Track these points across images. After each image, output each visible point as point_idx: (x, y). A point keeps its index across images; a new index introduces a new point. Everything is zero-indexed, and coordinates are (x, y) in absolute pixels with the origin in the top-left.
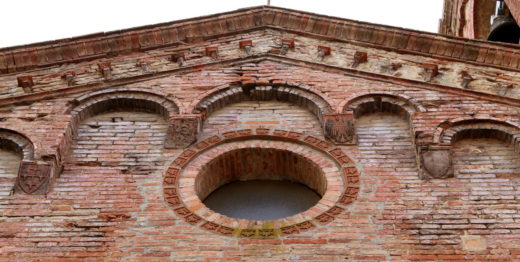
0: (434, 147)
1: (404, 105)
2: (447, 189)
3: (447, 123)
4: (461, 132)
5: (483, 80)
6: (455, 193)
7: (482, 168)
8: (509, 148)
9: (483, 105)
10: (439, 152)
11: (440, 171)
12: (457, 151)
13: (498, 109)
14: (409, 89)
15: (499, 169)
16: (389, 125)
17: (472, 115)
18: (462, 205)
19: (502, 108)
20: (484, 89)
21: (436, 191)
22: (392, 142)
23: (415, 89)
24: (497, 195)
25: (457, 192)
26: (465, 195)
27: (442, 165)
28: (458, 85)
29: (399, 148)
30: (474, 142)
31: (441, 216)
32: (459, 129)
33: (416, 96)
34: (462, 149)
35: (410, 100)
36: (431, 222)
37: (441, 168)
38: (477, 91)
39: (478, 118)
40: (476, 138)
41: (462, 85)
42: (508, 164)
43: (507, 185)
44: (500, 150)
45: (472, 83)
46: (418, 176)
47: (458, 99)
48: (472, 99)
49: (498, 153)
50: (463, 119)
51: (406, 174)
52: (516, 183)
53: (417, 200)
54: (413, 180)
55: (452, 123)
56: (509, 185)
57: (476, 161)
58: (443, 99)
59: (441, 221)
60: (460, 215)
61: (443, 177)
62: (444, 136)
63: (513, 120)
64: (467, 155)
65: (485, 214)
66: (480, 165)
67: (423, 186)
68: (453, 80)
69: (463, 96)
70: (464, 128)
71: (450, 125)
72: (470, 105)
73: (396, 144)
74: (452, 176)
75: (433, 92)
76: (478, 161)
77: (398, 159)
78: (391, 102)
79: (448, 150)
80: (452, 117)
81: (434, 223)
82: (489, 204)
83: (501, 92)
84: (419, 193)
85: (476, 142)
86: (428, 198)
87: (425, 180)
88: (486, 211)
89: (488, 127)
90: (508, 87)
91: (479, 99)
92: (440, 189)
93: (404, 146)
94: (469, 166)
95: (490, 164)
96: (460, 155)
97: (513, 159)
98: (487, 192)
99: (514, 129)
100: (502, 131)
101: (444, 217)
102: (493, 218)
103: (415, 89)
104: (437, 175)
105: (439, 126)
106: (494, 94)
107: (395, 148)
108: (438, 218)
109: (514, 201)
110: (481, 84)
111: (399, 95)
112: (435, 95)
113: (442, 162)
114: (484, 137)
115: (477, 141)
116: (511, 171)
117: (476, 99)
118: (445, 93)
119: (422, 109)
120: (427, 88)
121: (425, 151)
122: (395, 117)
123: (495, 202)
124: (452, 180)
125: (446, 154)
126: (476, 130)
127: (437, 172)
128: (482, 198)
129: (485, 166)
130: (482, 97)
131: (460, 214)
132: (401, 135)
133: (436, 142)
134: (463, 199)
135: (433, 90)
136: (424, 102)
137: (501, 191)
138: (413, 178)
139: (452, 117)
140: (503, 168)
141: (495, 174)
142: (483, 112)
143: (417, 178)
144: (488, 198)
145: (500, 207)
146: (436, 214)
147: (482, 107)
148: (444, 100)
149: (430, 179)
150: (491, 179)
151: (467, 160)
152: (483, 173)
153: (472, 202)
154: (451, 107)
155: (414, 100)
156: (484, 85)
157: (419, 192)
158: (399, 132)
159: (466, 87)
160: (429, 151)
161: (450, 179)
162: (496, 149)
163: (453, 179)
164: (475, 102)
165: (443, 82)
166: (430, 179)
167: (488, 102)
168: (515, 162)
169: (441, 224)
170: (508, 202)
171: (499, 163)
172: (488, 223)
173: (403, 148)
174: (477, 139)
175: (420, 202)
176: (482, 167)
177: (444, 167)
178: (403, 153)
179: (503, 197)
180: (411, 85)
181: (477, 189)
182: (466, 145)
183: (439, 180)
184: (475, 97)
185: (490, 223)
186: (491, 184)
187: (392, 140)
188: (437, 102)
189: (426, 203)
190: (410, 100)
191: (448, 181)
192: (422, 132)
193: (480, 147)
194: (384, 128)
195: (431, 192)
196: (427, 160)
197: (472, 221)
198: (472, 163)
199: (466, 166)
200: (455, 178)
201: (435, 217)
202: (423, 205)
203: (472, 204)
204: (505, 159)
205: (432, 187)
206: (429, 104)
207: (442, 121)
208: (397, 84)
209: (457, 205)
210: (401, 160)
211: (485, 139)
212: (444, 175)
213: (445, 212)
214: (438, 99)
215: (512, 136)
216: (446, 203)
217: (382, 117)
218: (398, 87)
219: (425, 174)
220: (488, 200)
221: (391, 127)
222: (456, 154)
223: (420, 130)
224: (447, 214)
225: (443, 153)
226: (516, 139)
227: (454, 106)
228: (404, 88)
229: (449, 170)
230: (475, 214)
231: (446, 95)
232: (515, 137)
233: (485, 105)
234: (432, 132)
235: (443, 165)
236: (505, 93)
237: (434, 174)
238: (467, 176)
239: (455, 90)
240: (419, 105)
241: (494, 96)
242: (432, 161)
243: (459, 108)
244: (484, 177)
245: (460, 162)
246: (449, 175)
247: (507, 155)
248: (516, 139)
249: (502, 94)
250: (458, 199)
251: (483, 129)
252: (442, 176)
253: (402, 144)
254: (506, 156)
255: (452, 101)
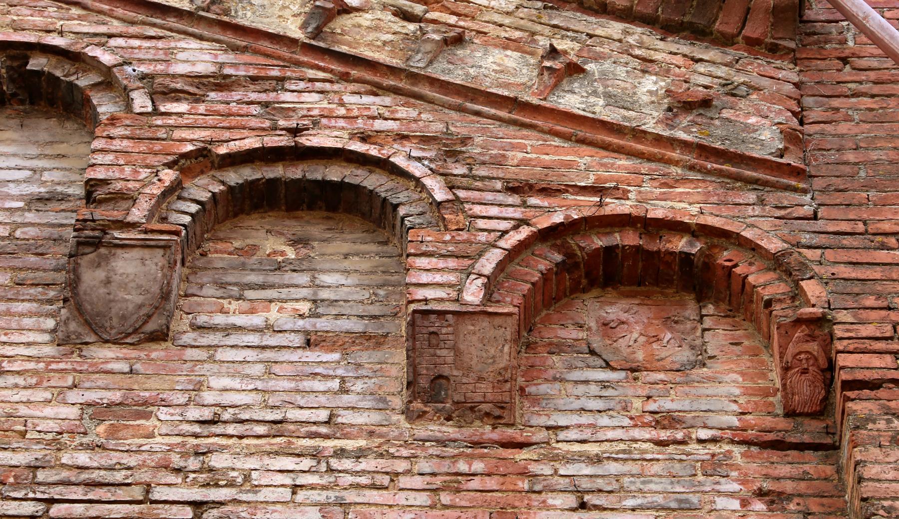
0: (123, 236)
1: (95, 86)
2: (126, 381)
3: (205, 156)
4: (241, 186)
5: (379, 14)
6: (147, 394)
7: (273, 314)
8: (389, 249)
9: (347, 98)
10: (136, 253)
11: (124, 318)
12: (216, 252)
13: (387, 114)
14: (133, 30)
15: (323, 319)
16: (34, 151)
17: (295, 132)
18: (151, 436)
19: (403, 112)
20: (370, 45)
21: (87, 385)
22: (18, 209)
23: (152, 32)
24: (278, 407)
25: (154, 393)
26: (175, 402)
27: (135, 298)
28: (293, 27)
29: (32, 232)
30: (287, 222)
31: (65, 474)
32: (234, 177)
33: (141, 56)
34: (237, 244)
35: (115, 70)
36: (20, 495)
37: (131, 307)
38: (344, 49)
39: (308, 144)
40: (297, 209)
41: (303, 27)
42: (362, 302)
43: (325, 372)
44: (354, 255)
45: (344, 22)
46: (54, 331)
47: (275, 72)
48: (321, 75)
49: (346, 264)
50: (258, 145)
51: (14, 325)
52: (359, 366)
53: (10, 416)
54: (29, 344)
55: (218, 155)
56: (331, 373)
57: (263, 287)
58: (227, 71)
59: (55, 492)
60: (129, 472)
61: (128, 340)
62: (180, 198)
63: (415, 153)
64: (243, 267)
65: (211, 470)
66: (271, 301)
67: (54, 366)
68: (284, 7)
69: (298, 64)
70: (258, 176)
71: (212, 163)
72: (306, 97)
73: (30, 217)
74: (160, 336)
75: (206, 45)
76: (272, 286)
77: (14, 269)
78: (58, 73)
79: (166, 247)
80: (227, 135)
81: (31, 495)
82: (241, 437)
83: (419, 56)
84: (29, 392)
85: (293, 223)
86: (48, 411)
87: (67, 347)
88: (217, 461)
89: (334, 173)
90: (446, 41)
91: (345, 77)
92: (102, 380)
93: (53, 226)
94: (235, 305)
95: (304, 299)
96: (220, 265)
97: (381, 286)
98: (253, 394)
99: (412, 184)
100: (371, 191)
101: (72, 475)
102: (231, 484)
103: (152, 32)
104: (113, 332)
105: (169, 165)
106: (395, 62)
107: (18, 233)
108: (50, 480)
109: (323, 430)
110: (368, 28)
111: (86, 50)
112: (208, 57)
113: (139, 287)
114: (320, 208)
115: (296, 218)
116: (357, 326)
117: (334, 78)
118: (245, 49)
119: (141, 101)
120: (191, 30)
121: (87, 250)
122: (68, 125)
123: (261, 429)
124: (157, 352)
125: (155, 261)
126: (294, 181)
127: (115, 321)
128: (226, 416)
129: (285, 305)
130: (353, 72)
131: (129, 468)
132: (59, 189)
133: (136, 219)
134: (162, 417)
135: (208, 40)
136: (159, 80)
137: (298, 391)
138: (32, 337)
139: (227, 135)
140: (338, 316)
141: (307, 333)
142: (333, 122)
143: (46, 337)
144: (245, 416)
145: (268, 448)
146: (52, 467)
147: (342, 104)
148: (230, 76)
149: (87, 343)
150: (284, 351)
151: (236, 284)
152: (269, 328)
153: (186, 428)
154: (239, 102)
155: (129, 69)
156: (377, 29)
157: (30, 387)
158: (57, 176)
159: (317, 33)
160: (103, 250)
161: (154, 346)
162: (346, 247)
163: (164, 345)
164: (328, 86)
165: (249, 14)
166: (87, 343)
167: (369, 87)
168: (387, 296)
169: (52, 501)
170: (304, 430)
171: (333, 297)
172: (206, 503)
173: (47, 232)
174: (299, 213)
175: (15, 423)
176: (274, 307)
177: (140, 307)
178: (39, 251)
179: (293, 414)
180: (141, 17)
181: (227, 382)
182: (254, 233)
183: (114, 347)
184: (331, 71)
185: (214, 502)
186: (276, 369)
187: (21, 204)
188: (205, 80)
189: (35, 425)
190: (115, 70)
191: (143, 354)
192: (105, 182)
193: (297, 242)
194: (13, 162)
195: (70, 388)
196: (91, 278)
197: (159, 494)
198: (250, 294)
199: (225, 302)
200: (169, 344)
201: (41, 476)
202: (23, 434)
203: (183, 435)
204: (357, 286)
205: (81, 372)
206: (173, 85)
207: (189, 148)
208: (100, 12)
209: (133, 436)
210: (22, 275)
211: (325, 214)
212: (136, 331)
213: (83, 458)
214: (211, 69)
215: (396, 207)
216: (101, 429)
217: (26, 122)
218: (98, 23)
219: (73, 326)
220: (242, 422)
221: (38, 157)
222: (209, 262)
223: (101, 176)
224: (87, 468)
225: (147, 257)
226: (403, 219)
227: (253, 96)
228: (116, 26)
229: (154, 318)
230: (178, 471)
231: (247, 58)
232: (402, 211)
233: (355, 99)
234: (137, 185)
235: (139, 299)
236: (431, 62)
237: (103, 326)
238: (212, 337)
239: (278, 43)
240: (138, 88)
241: (392, 70)
242: (108, 282)
243: (266, 105)
244: (264, 343)
245: (209, 290)
246: (152, 333)
247: (372, 273)
248: (403, 219)
249: (418, 64)
250: (147, 416)
251: (316, 182)
252: (128, 335)
253: (52, 218)
254: (367, 273)
255: (254, 79)
